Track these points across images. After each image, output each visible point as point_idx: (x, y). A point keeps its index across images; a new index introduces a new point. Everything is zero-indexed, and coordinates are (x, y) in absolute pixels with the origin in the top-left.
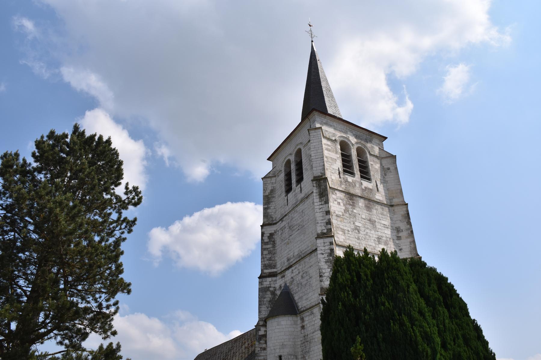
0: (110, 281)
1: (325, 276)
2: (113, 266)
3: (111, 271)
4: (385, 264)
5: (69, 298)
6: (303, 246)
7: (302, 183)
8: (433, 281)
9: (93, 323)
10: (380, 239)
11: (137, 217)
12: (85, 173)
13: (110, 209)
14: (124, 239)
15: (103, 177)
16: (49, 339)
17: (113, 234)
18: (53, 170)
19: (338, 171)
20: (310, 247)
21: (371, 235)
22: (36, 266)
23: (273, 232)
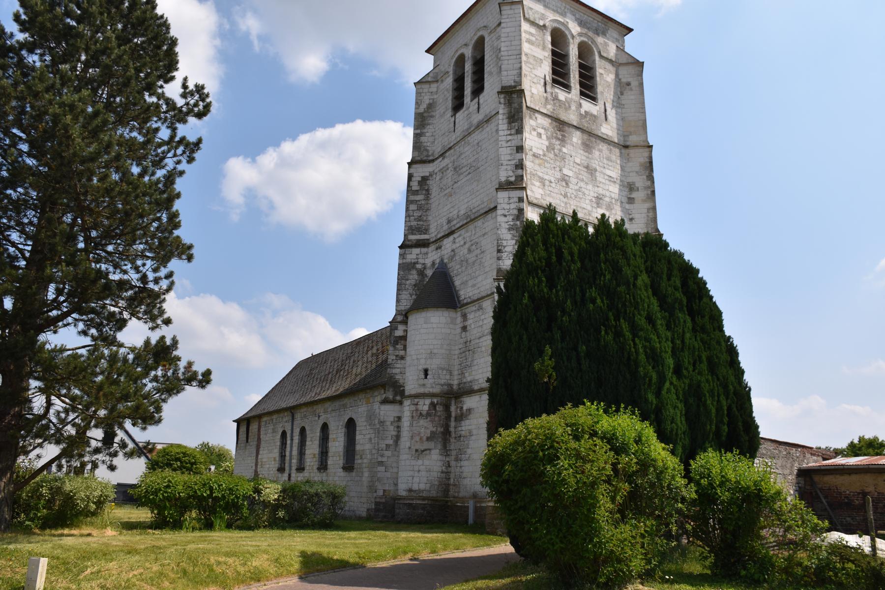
0: (160, 239)
1: (505, 252)
2: (164, 215)
3: (161, 224)
4: (603, 238)
5: (93, 264)
6: (474, 201)
7: (481, 96)
8: (675, 272)
9: (134, 304)
10: (601, 199)
11: (203, 138)
12: (112, 57)
13: (156, 122)
14: (182, 173)
15: (144, 65)
16: (65, 326)
17: (163, 164)
18: (55, 48)
19: (542, 81)
20: (486, 204)
21: (587, 192)
22: (36, 212)
23: (427, 174)
